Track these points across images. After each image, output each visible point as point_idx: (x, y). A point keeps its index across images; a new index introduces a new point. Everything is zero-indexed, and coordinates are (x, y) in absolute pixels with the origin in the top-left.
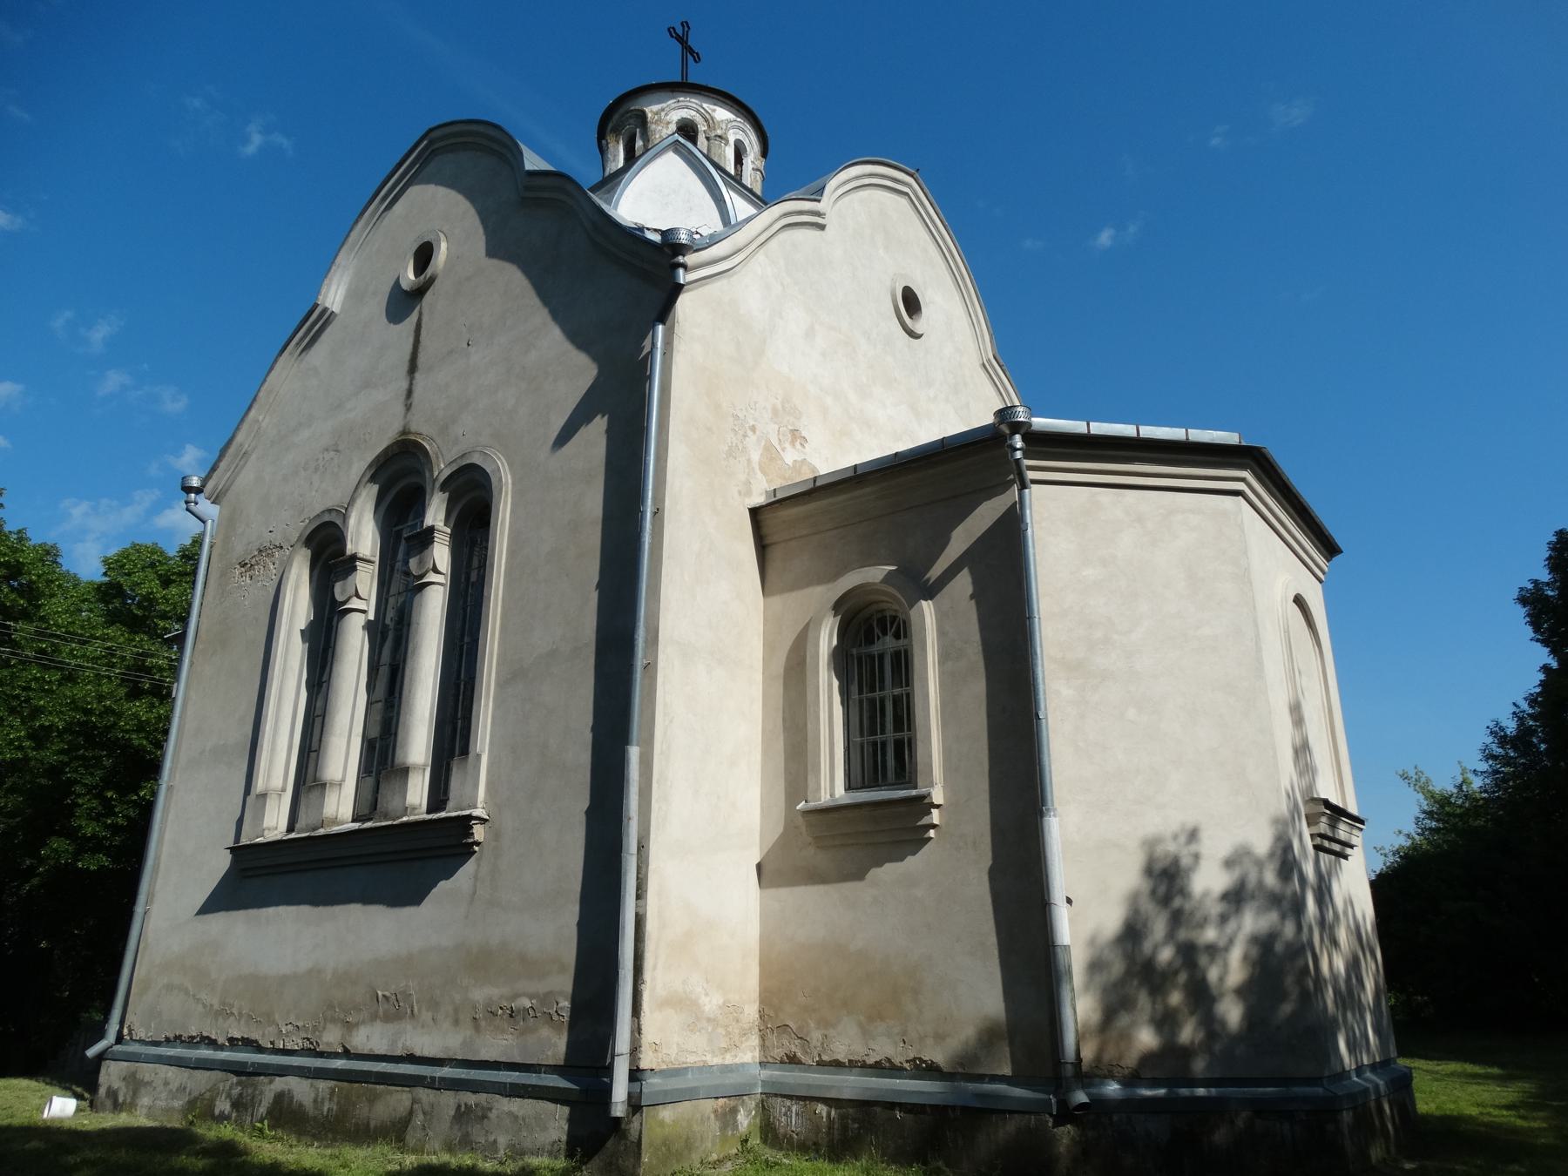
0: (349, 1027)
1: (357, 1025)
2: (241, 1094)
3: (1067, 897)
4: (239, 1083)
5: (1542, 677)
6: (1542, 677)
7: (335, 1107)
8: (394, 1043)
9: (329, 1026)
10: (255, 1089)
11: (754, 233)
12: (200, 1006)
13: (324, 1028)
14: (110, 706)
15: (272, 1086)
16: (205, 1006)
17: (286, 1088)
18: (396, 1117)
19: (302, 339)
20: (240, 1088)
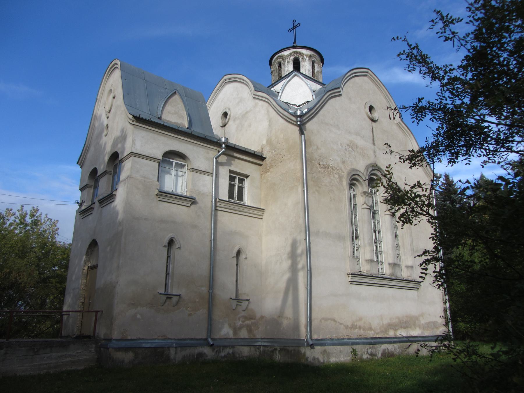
0: (396, 330)
1: (397, 329)
2: (372, 352)
3: (249, 176)
4: (370, 348)
5: (424, 251)
6: (424, 251)
7: (400, 350)
8: (407, 334)
9: (390, 330)
10: (376, 349)
11: (277, 108)
12: (342, 326)
13: (389, 331)
14: (476, 362)
15: (381, 348)
16: (344, 326)
17: (386, 348)
18: (383, 324)
19: (106, 76)
20: (370, 350)
